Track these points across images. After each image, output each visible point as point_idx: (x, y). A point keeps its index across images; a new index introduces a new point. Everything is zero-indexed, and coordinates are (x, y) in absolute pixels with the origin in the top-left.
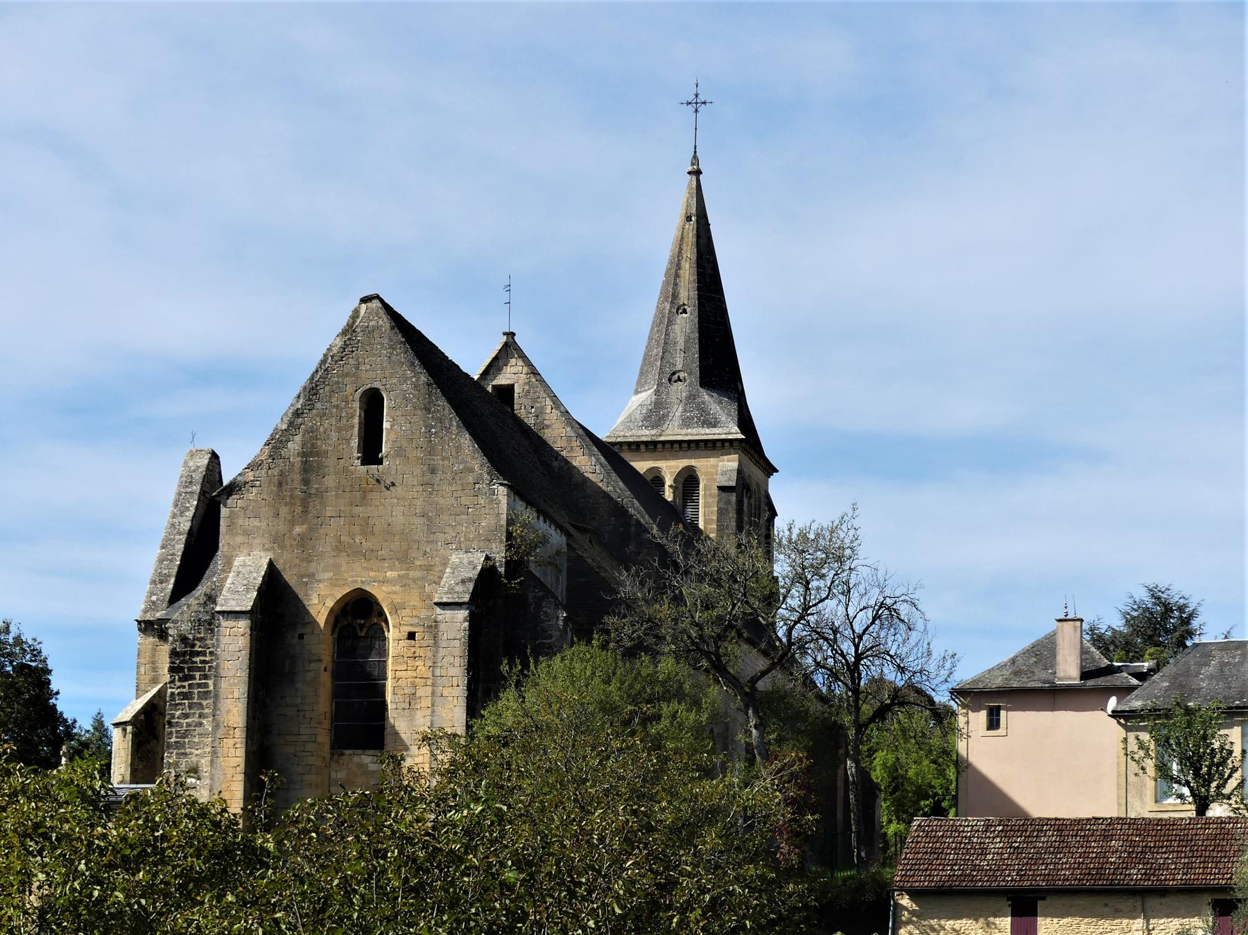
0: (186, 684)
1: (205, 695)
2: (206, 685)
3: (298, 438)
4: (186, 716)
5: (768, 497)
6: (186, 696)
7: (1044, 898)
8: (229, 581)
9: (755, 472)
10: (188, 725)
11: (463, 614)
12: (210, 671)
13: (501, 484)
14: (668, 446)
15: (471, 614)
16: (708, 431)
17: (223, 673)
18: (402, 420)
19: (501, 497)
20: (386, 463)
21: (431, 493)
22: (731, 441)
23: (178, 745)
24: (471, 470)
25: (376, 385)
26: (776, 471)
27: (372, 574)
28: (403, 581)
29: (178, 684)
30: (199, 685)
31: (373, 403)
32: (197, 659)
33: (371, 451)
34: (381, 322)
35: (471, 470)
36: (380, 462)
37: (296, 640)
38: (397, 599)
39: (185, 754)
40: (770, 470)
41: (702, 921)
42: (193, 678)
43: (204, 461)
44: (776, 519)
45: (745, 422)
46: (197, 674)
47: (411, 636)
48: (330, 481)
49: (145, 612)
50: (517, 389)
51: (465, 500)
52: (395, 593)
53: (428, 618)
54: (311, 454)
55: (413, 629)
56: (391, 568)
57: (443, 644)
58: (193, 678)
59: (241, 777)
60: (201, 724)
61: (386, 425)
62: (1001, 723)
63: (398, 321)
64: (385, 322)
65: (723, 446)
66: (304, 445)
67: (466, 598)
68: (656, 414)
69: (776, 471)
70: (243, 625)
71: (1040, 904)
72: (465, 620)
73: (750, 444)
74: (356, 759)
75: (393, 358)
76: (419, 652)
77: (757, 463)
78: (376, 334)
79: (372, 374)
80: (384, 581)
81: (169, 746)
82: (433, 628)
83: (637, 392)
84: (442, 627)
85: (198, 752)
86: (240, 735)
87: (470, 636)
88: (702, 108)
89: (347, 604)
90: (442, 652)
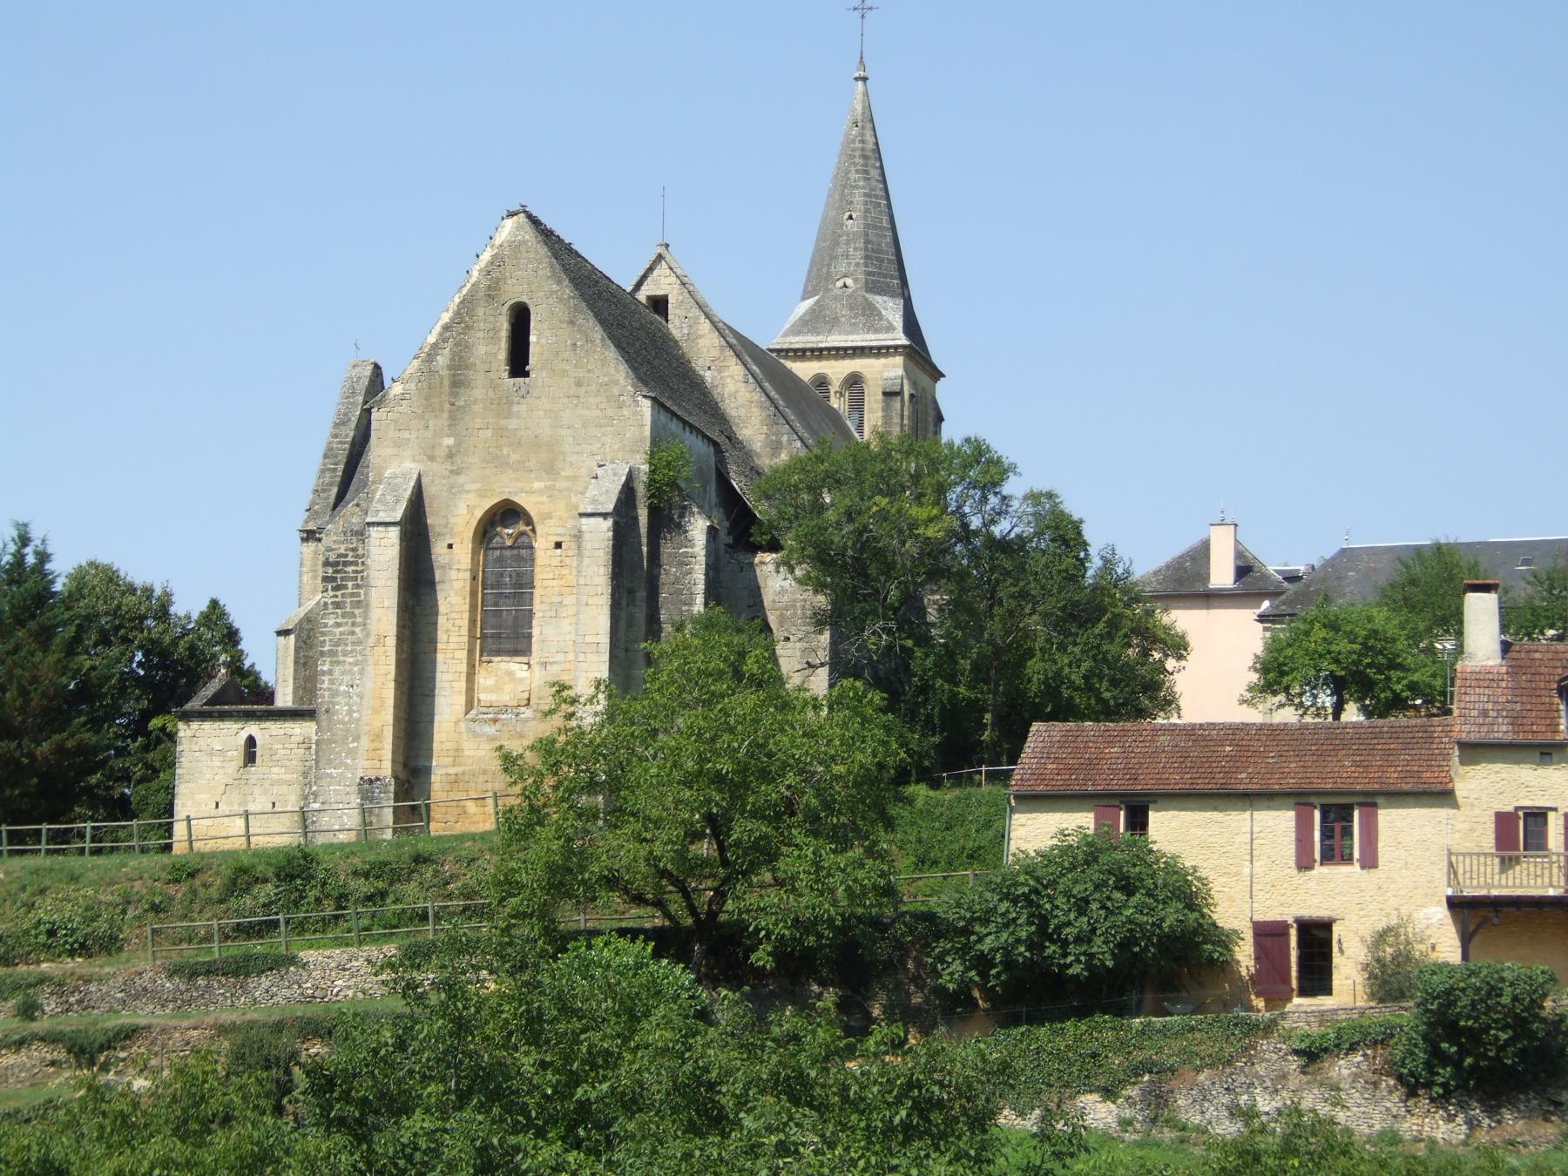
0: (339, 593)
1: (358, 604)
2: (358, 595)
3: (446, 351)
4: (338, 625)
5: (935, 402)
6: (337, 605)
7: (1155, 802)
8: (379, 493)
9: (924, 379)
10: (341, 633)
11: (610, 522)
12: (362, 582)
13: (645, 396)
14: (858, 352)
15: (616, 524)
16: (873, 337)
17: (373, 583)
18: (547, 333)
19: (644, 409)
20: (532, 375)
21: (576, 406)
22: (896, 347)
23: (332, 653)
24: (616, 383)
25: (524, 299)
26: (943, 376)
27: (519, 485)
28: (551, 492)
29: (331, 593)
30: (352, 595)
31: (520, 319)
32: (350, 569)
33: (518, 363)
34: (527, 237)
35: (616, 383)
36: (526, 374)
37: (446, 550)
38: (545, 509)
39: (339, 663)
40: (937, 375)
41: (1165, 880)
42: (345, 587)
43: (368, 371)
44: (944, 425)
45: (911, 326)
46: (350, 584)
47: (558, 545)
48: (478, 393)
49: (306, 522)
50: (671, 300)
51: (609, 412)
52: (541, 503)
53: (575, 527)
54: (459, 367)
55: (559, 539)
56: (539, 479)
57: (586, 553)
58: (345, 587)
59: (392, 685)
60: (353, 633)
61: (533, 338)
62: (394, 584)
63: (547, 235)
64: (529, 235)
65: (821, 354)
66: (452, 360)
67: (610, 507)
68: (812, 321)
69: (943, 376)
70: (394, 534)
71: (1151, 806)
72: (609, 530)
73: (917, 352)
74: (503, 666)
75: (540, 272)
76: (567, 561)
77: (923, 369)
78: (523, 249)
79: (517, 289)
80: (531, 492)
81: (322, 654)
82: (578, 536)
83: (804, 299)
84: (587, 536)
85: (351, 660)
86: (392, 641)
87: (614, 546)
88: (868, 14)
89: (495, 514)
90: (586, 561)
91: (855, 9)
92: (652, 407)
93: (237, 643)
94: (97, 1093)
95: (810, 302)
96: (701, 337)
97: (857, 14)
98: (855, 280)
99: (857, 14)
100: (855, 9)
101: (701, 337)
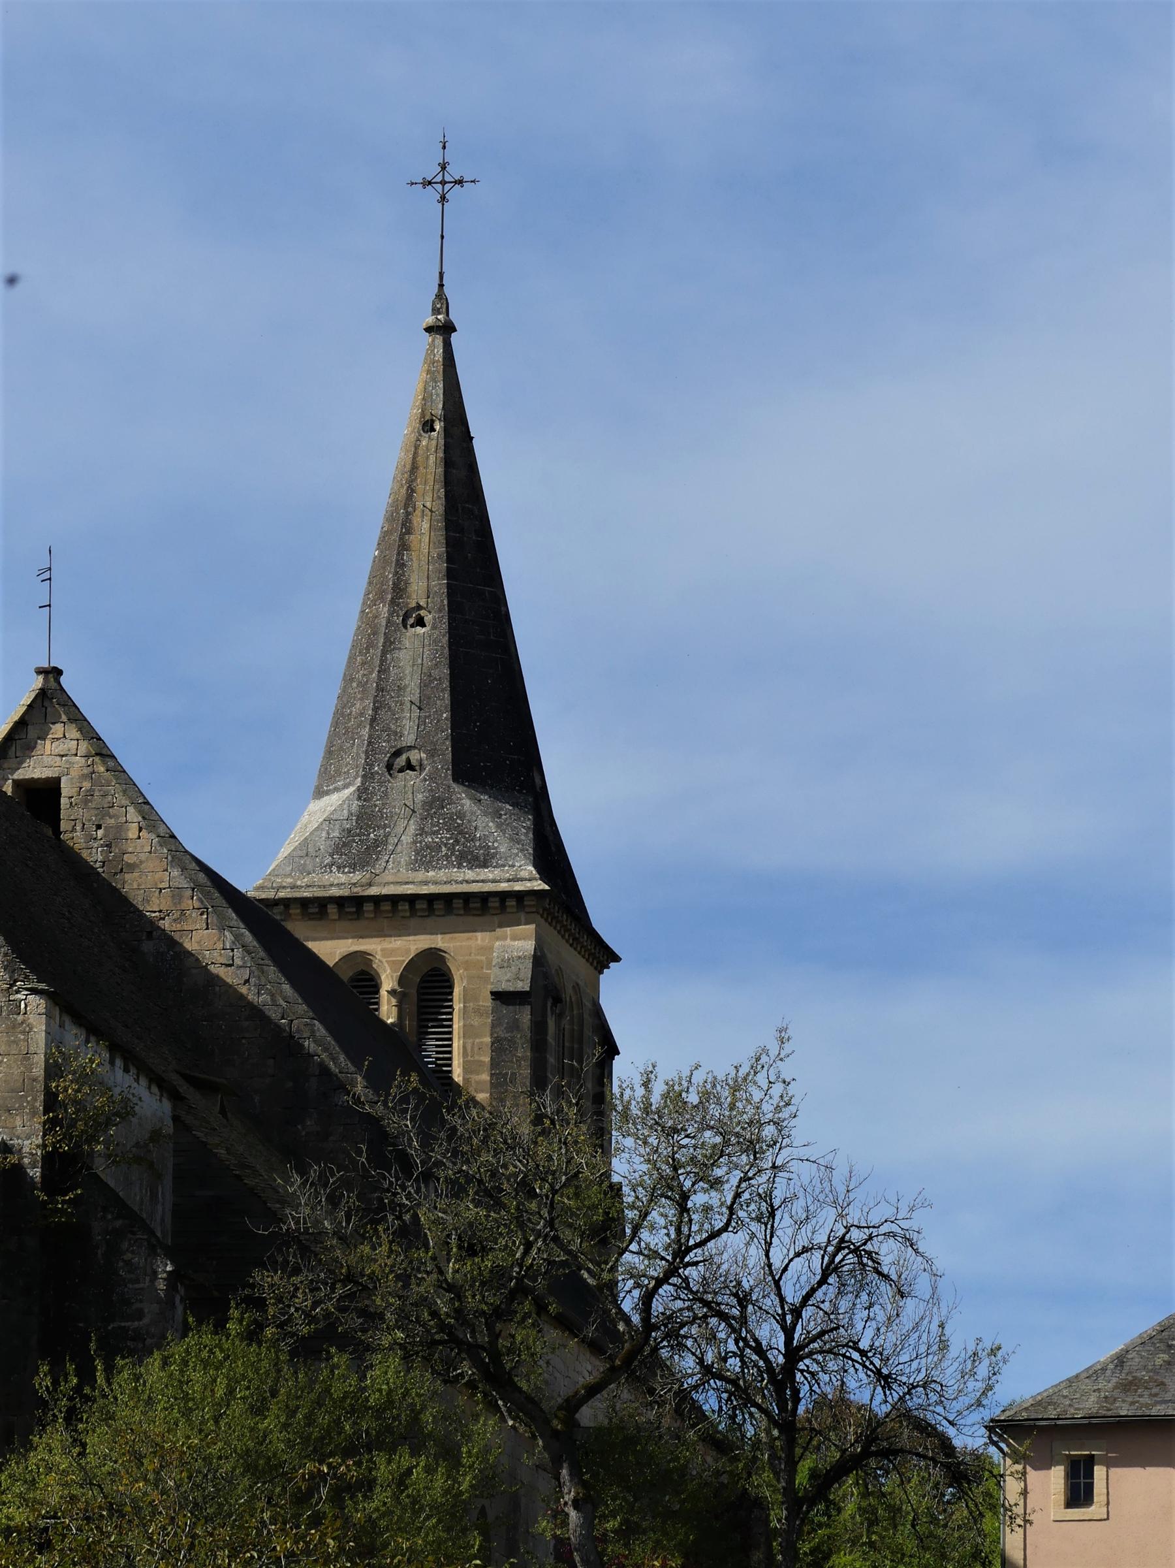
9: (572, 961)
13: (33, 991)
22: (520, 896)
26: (617, 959)
40: (603, 956)
44: (617, 1062)
50: (66, 789)
69: (617, 959)
77: (574, 942)
83: (319, 793)
88: (455, 193)
91: (460, 182)
92: (49, 1015)
93: (174, 1116)
94: (482, 1401)
95: (334, 801)
96: (132, 867)
97: (433, 193)
98: (432, 754)
99: (433, 193)
100: (460, 182)
101: (132, 867)
